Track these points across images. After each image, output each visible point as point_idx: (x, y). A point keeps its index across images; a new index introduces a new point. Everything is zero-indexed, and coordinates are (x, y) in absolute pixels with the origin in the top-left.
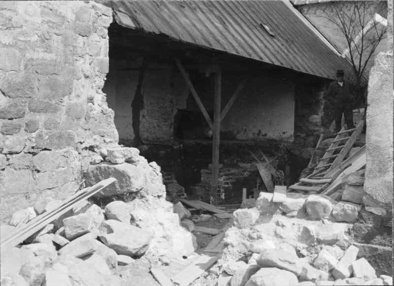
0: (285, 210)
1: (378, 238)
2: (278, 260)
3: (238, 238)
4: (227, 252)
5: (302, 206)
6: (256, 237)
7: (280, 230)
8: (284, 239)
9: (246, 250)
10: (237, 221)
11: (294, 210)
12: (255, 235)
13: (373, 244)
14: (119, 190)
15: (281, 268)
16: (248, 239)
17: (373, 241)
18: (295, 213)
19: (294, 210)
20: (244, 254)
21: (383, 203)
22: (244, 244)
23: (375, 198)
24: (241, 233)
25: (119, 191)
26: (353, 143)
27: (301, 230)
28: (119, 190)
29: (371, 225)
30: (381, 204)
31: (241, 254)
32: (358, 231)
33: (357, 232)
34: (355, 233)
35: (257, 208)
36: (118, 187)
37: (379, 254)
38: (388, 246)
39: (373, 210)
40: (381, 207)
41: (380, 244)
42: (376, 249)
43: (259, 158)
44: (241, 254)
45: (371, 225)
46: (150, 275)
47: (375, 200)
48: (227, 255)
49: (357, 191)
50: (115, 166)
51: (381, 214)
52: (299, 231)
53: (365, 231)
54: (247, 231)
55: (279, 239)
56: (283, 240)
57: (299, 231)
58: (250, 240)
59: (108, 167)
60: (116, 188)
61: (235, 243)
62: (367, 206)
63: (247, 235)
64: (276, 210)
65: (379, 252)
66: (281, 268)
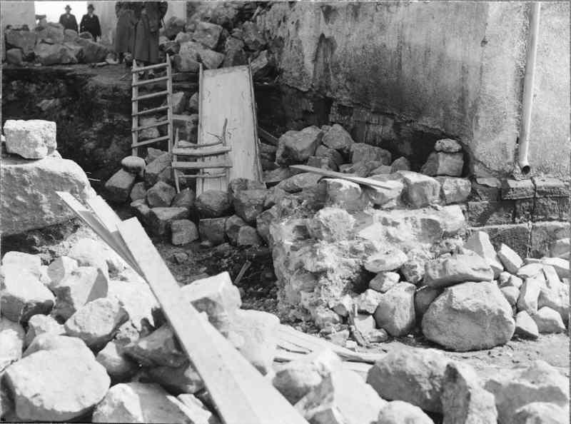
0: (378, 201)
1: (494, 217)
2: (472, 271)
3: (337, 258)
4: (328, 283)
5: (401, 190)
6: (363, 249)
7: (391, 230)
8: (403, 242)
9: (350, 272)
10: (327, 230)
11: (392, 199)
12: (361, 247)
13: (489, 224)
14: (52, 215)
15: (478, 281)
16: (351, 255)
17: (312, 195)
18: (394, 203)
19: (392, 199)
20: (349, 279)
21: (496, 171)
22: (347, 265)
23: (488, 166)
24: (339, 248)
25: (51, 219)
26: (271, 11)
27: (419, 224)
28: (52, 215)
29: (487, 202)
30: (494, 173)
31: (344, 281)
32: (474, 212)
33: (472, 214)
34: (470, 215)
35: (339, 204)
36: (47, 211)
37: (499, 235)
38: (504, 223)
39: (486, 182)
40: (494, 176)
41: (497, 223)
42: (496, 230)
43: (142, 73)
44: (344, 281)
45: (487, 202)
46: (282, 350)
47: (489, 168)
48: (330, 288)
49: (455, 160)
50: (36, 164)
51: (495, 186)
52: (417, 227)
53: (480, 210)
54: (346, 244)
55: (396, 244)
56: (402, 244)
57: (417, 227)
58: (355, 256)
59: (18, 170)
60: (44, 213)
61: (335, 267)
62: (479, 177)
63: (348, 249)
64: (366, 203)
65: (499, 233)
66: (478, 281)
